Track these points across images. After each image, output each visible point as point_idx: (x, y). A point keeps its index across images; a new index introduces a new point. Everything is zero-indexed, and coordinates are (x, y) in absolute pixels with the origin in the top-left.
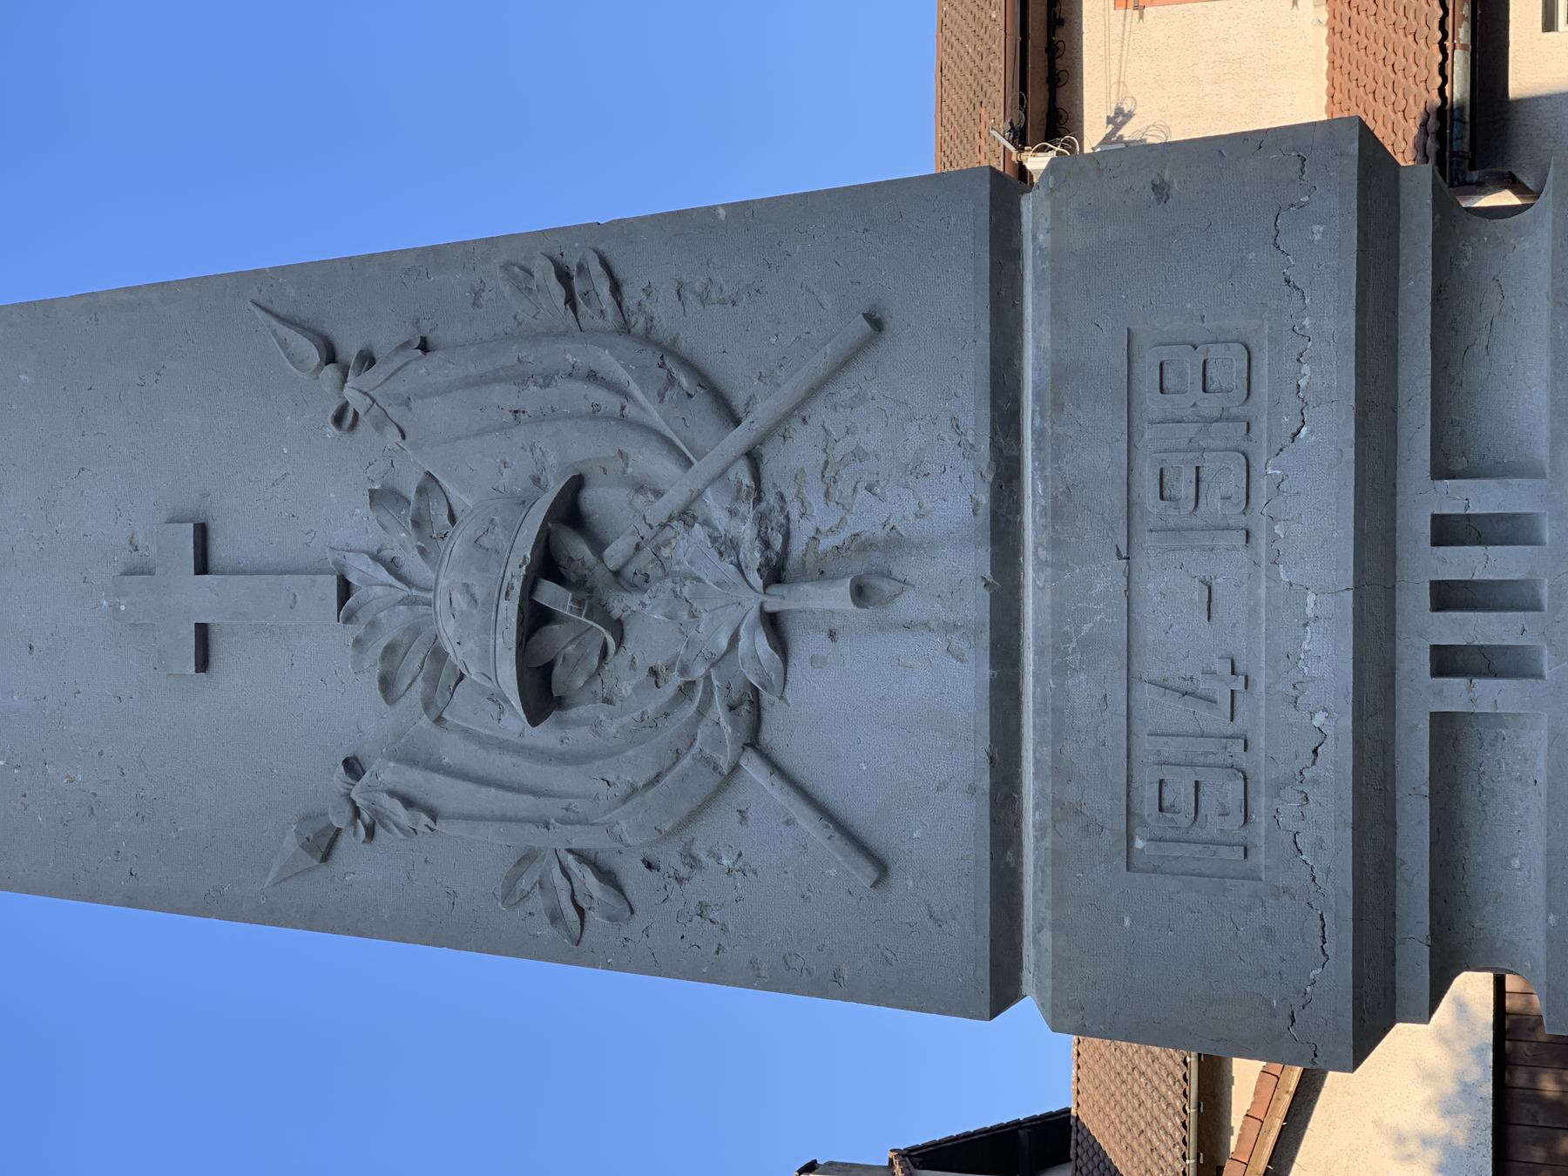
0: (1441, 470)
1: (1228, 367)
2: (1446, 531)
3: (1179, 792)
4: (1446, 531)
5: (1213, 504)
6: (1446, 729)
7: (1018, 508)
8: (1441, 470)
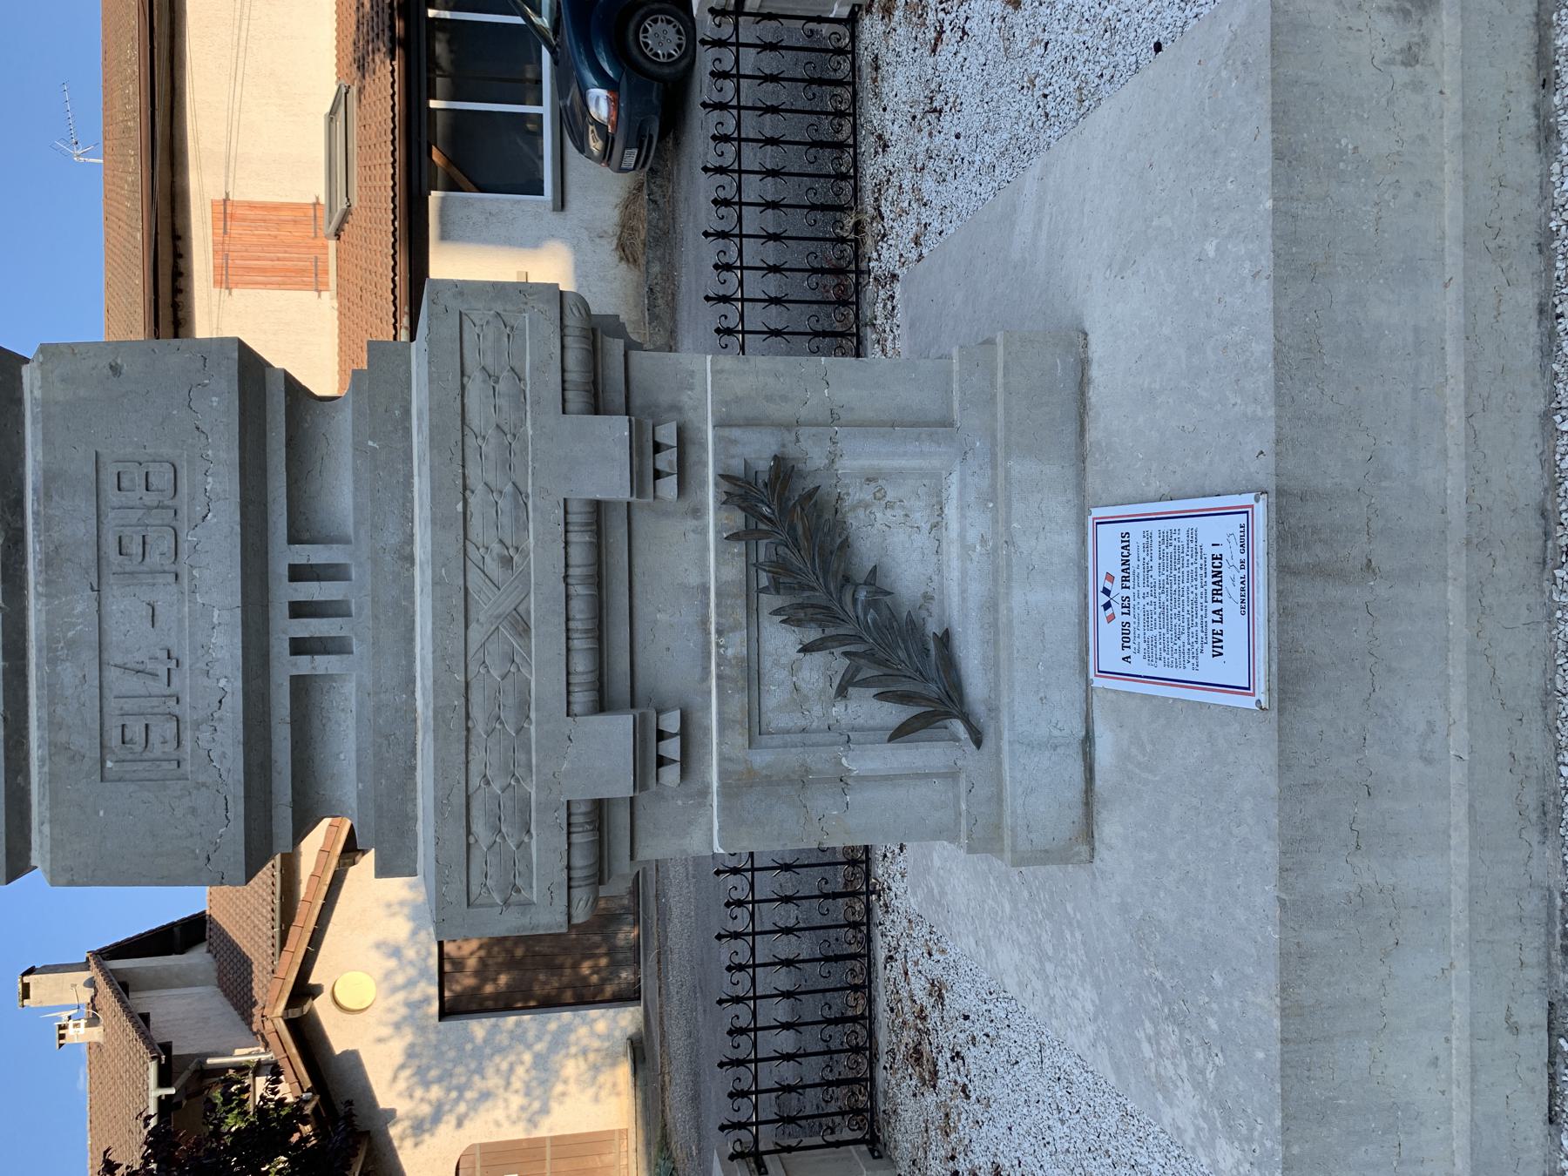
0: (294, 539)
1: (160, 479)
2: (298, 573)
3: (136, 731)
4: (298, 573)
5: (154, 559)
6: (301, 685)
7: (23, 560)
8: (294, 539)
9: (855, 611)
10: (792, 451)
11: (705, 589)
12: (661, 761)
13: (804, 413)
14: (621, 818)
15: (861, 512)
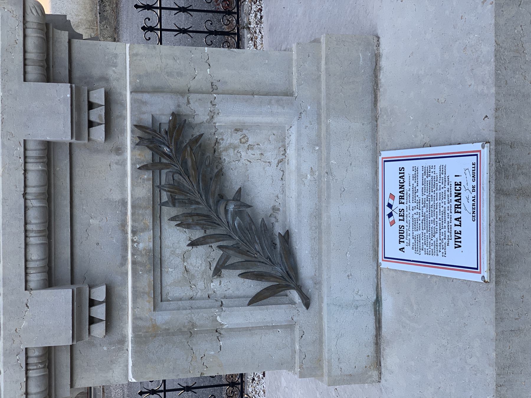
9: (226, 217)
10: (185, 110)
11: (124, 203)
12: (92, 321)
13: (193, 84)
14: (64, 359)
15: (231, 152)
